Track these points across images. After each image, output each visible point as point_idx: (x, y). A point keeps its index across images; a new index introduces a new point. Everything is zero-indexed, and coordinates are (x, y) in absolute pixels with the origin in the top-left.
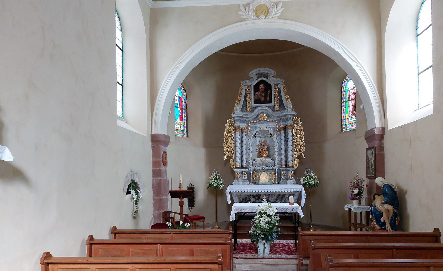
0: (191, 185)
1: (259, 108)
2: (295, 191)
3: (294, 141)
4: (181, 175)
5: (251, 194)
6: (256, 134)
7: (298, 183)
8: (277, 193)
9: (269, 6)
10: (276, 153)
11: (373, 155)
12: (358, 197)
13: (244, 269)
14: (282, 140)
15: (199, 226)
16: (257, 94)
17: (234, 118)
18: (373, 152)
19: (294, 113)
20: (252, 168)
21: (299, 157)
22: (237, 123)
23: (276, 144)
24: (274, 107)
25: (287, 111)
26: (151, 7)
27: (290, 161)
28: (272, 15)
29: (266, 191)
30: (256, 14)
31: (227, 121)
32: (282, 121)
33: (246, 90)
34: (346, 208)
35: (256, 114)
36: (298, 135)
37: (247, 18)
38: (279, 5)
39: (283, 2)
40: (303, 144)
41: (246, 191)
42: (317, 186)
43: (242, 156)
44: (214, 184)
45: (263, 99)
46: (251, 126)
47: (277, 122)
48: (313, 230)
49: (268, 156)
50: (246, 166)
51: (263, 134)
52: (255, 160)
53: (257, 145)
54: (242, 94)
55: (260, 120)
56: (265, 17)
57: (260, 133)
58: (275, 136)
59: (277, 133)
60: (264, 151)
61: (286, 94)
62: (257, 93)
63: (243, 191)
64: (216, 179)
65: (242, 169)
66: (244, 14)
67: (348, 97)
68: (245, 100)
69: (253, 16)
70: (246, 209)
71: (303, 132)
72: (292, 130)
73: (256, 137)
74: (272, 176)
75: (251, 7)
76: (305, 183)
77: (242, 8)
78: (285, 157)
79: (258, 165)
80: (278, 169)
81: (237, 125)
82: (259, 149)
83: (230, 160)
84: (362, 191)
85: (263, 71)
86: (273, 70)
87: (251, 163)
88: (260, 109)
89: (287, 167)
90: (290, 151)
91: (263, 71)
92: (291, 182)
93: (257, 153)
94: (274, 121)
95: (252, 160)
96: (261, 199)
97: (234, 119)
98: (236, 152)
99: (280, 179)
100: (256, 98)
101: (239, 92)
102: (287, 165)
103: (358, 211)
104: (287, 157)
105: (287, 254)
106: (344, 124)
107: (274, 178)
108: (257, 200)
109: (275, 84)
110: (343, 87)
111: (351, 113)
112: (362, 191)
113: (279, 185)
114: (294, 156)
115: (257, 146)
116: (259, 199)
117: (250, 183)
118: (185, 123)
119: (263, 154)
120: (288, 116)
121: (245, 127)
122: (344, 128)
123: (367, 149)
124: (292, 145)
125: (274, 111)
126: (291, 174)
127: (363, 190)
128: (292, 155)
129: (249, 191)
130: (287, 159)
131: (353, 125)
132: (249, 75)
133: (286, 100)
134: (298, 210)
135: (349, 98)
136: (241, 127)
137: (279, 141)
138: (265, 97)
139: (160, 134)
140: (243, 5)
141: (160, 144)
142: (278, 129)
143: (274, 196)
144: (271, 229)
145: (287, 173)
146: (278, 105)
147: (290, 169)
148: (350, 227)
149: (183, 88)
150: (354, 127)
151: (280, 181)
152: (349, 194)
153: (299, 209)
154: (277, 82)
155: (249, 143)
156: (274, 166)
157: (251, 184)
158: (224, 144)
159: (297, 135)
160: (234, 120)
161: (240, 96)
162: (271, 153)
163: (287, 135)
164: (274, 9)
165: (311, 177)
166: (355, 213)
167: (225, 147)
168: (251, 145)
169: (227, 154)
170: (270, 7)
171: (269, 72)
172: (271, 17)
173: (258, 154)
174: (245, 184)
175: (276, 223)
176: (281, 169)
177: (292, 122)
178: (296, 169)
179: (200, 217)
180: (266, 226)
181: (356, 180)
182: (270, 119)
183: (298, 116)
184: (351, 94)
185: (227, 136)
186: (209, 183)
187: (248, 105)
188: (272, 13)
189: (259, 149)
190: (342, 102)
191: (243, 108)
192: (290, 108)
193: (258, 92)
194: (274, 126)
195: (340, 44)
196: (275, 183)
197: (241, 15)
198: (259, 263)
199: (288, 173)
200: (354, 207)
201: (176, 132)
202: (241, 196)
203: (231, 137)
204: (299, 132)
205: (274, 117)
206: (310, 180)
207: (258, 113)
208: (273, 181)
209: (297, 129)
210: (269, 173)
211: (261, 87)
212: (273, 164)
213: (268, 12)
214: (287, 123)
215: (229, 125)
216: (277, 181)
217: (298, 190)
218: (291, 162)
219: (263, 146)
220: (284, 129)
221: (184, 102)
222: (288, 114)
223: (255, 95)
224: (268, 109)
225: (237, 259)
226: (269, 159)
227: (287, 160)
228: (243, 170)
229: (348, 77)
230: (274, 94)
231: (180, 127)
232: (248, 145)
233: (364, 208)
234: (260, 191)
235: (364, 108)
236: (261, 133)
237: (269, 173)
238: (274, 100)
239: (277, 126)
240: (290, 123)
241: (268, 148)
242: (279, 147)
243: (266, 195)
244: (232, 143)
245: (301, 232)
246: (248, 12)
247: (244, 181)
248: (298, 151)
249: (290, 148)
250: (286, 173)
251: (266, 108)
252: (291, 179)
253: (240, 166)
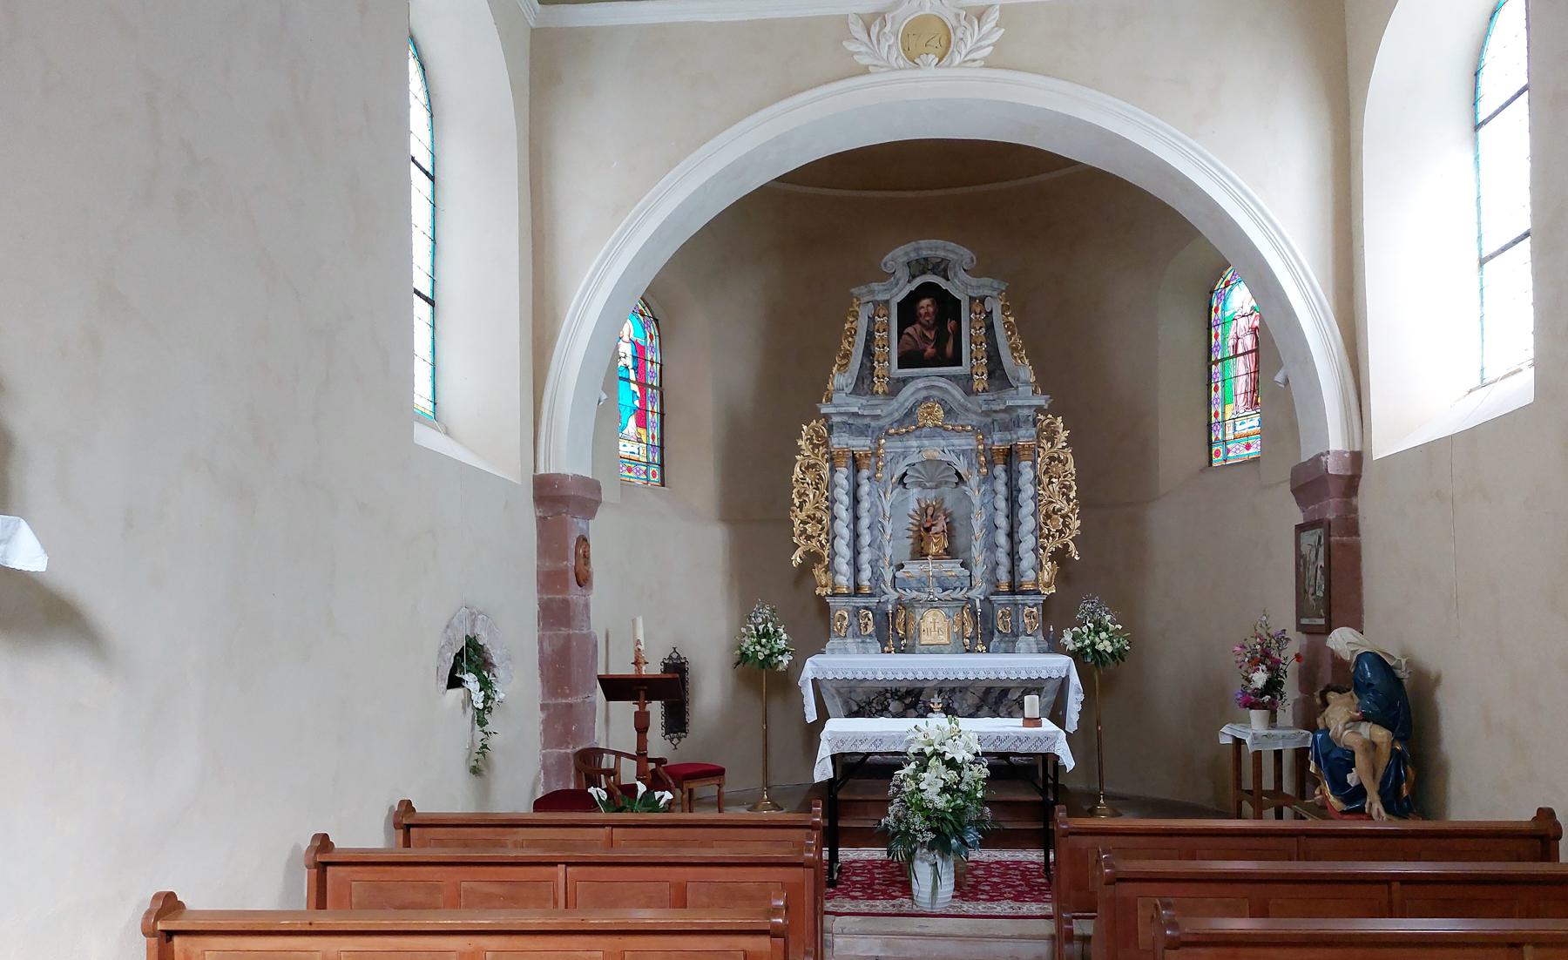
0: (675, 656)
1: (918, 381)
2: (1044, 675)
3: (1040, 501)
4: (640, 621)
5: (888, 685)
6: (905, 474)
7: (1055, 647)
8: (980, 684)
9: (951, 21)
10: (979, 542)
11: (1322, 550)
12: (1267, 698)
13: (863, 952)
14: (999, 496)
15: (705, 801)
16: (908, 334)
17: (827, 416)
18: (1320, 538)
19: (1041, 401)
20: (893, 595)
21: (1060, 556)
22: (837, 435)
23: (977, 510)
24: (970, 378)
25: (1017, 394)
26: (533, 25)
27: (1026, 571)
28: (963, 53)
29: (941, 677)
30: (906, 50)
31: (805, 427)
32: (997, 428)
33: (871, 319)
34: (1226, 736)
35: (907, 404)
36: (1055, 478)
37: (875, 63)
38: (988, 18)
39: (1003, 8)
40: (1072, 511)
41: (870, 676)
42: (1123, 660)
43: (856, 553)
44: (756, 652)
45: (930, 350)
46: (889, 446)
47: (980, 433)
48: (1109, 813)
49: (950, 553)
50: (870, 588)
52: (902, 566)
53: (911, 513)
54: (856, 332)
55: (920, 424)
56: (937, 59)
57: (920, 472)
58: (974, 480)
59: (979, 471)
60: (936, 533)
61: (1013, 334)
62: (909, 330)
63: (860, 676)
64: (766, 635)
65: (856, 599)
66: (863, 49)
67: (1231, 342)
68: (868, 353)
69: (895, 56)
70: (871, 740)
71: (1071, 467)
72: (1034, 462)
73: (907, 486)
74: (963, 624)
75: (889, 25)
76: (1081, 649)
77: (857, 29)
78: (1009, 554)
80: (982, 598)
81: (840, 441)
82: (916, 529)
83: (816, 565)
84: (1282, 677)
85: (929, 252)
86: (965, 250)
87: (888, 577)
88: (921, 385)
89: (1016, 590)
90: (1027, 534)
91: (929, 252)
92: (1029, 645)
93: (911, 541)
94: (970, 428)
95: (892, 568)
96: (925, 707)
97: (827, 421)
98: (834, 538)
99: (992, 634)
100: (908, 348)
101: (847, 326)
102: (1016, 584)
103: (1268, 749)
104: (1017, 557)
105: (1015, 899)
106: (1217, 439)
107: (969, 630)
108: (909, 708)
109: (972, 299)
110: (1213, 309)
111: (1241, 399)
112: (1282, 677)
113: (987, 654)
114: (1041, 551)
115: (910, 516)
116: (917, 703)
117: (886, 649)
118: (653, 437)
119: (930, 544)
120: (1019, 411)
121: (868, 449)
122: (1217, 454)
123: (1300, 529)
124: (1034, 515)
125: (969, 392)
126: (1030, 615)
127: (1285, 672)
128: (1035, 550)
129: (880, 676)
130: (1016, 563)
131: (1250, 442)
132: (882, 265)
133: (1012, 354)
134: (1054, 745)
135: (1235, 347)
136: (854, 449)
137: (986, 501)
138: (940, 343)
139: (566, 476)
140: (861, 16)
141: (568, 511)
142: (983, 459)
143: (970, 694)
144: (958, 812)
145: (1017, 613)
146: (985, 371)
147: (1025, 597)
148: (1240, 803)
149: (647, 313)
150: (1252, 451)
151: (991, 641)
152: (1236, 686)
153: (1058, 741)
155: (880, 507)
156: (971, 589)
157: (890, 652)
158: (793, 512)
159: (1051, 477)
160: (829, 425)
161: (850, 339)
162: (960, 541)
163: (1017, 480)
164: (968, 34)
165: (1099, 627)
166: (1258, 755)
167: (797, 522)
168: (888, 515)
169: (803, 545)
170: (955, 23)
171: (951, 256)
172: (958, 60)
173: (912, 544)
174: (866, 652)
175: (975, 789)
176: (993, 598)
177: (1033, 431)
178: (1048, 597)
179: (707, 768)
180: (941, 802)
181: (1260, 636)
182: (956, 421)
183: (1054, 410)
184: (1242, 334)
185: (803, 483)
186: (740, 650)
187: (878, 371)
188: (963, 46)
189: (916, 529)
190: (1209, 363)
191: (860, 383)
192: (1027, 383)
193: (915, 326)
194: (970, 445)
195: (1204, 157)
196: (972, 648)
197: (852, 54)
198: (918, 930)
199: (1020, 612)
200: (1254, 734)
201: (624, 469)
202: (853, 695)
203: (817, 484)
204: (1057, 467)
205: (970, 415)
206: (1097, 639)
207: (912, 401)
208: (968, 640)
209: (1052, 459)
210: (951, 614)
211: (923, 307)
212: (966, 582)
213: (949, 42)
214: (1015, 436)
215: (811, 443)
216: (980, 641)
217: (1055, 675)
218: (1031, 575)
219: (932, 516)
220: (1007, 456)
221: (652, 362)
222: (1019, 403)
223: (903, 336)
224: (949, 388)
225: (838, 918)
226: (953, 565)
227: (1016, 568)
228: (860, 602)
229: (1233, 274)
230: (971, 335)
231: (637, 452)
232: (877, 514)
233: (1289, 738)
234: (920, 676)
235: (1287, 382)
236: (923, 472)
237: (951, 614)
238: (971, 353)
239: (980, 447)
240: (1028, 437)
241: (947, 523)
242: (986, 522)
243: (940, 692)
244: (820, 507)
245: (1066, 823)
246: (878, 41)
247: (863, 642)
248: (1053, 536)
249: (1028, 524)
250: (1013, 614)
251: (943, 383)
252: (1030, 635)
253: (848, 588)
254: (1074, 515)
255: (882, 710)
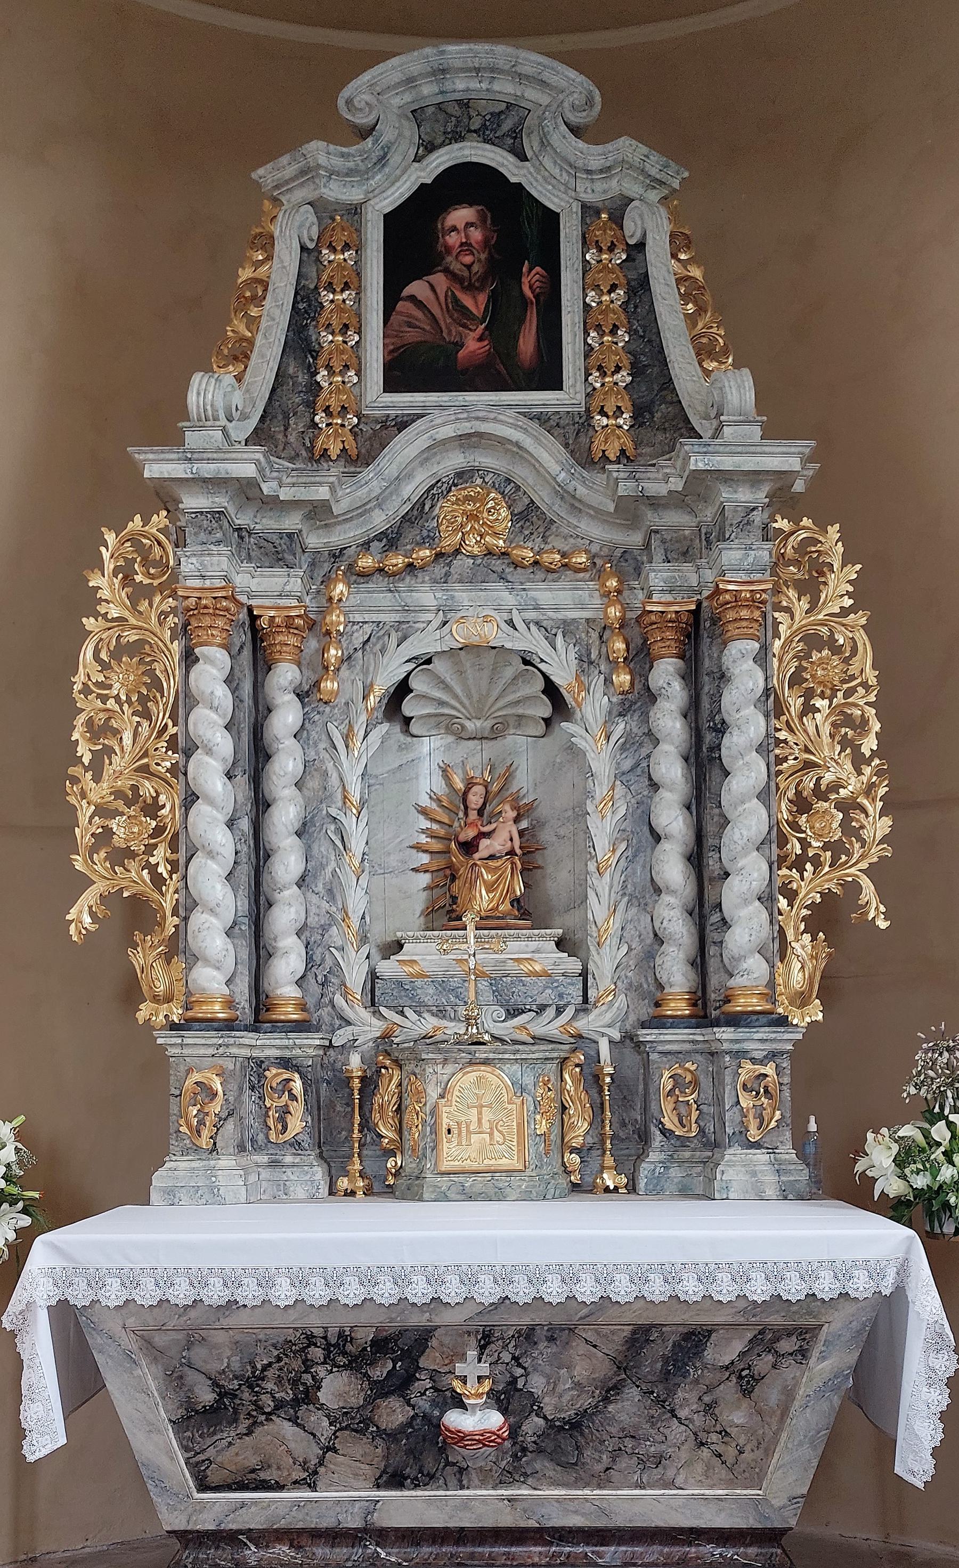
2: (826, 1287)
3: (780, 760)
5: (315, 1323)
6: (403, 689)
8: (611, 1314)
10: (607, 877)
14: (664, 747)
16: (412, 298)
23: (601, 790)
24: (584, 423)
29: (487, 1292)
31: (110, 537)
32: (658, 556)
40: (869, 790)
41: (249, 1293)
50: (303, 1007)
51: (476, 697)
52: (398, 946)
53: (425, 801)
54: (266, 290)
57: (447, 687)
59: (608, 681)
61: (701, 310)
62: (417, 288)
63: (215, 1294)
65: (249, 1038)
72: (765, 649)
73: (414, 728)
74: (564, 1108)
79: (428, 1000)
80: (617, 1036)
82: (437, 846)
85: (474, 84)
86: (572, 74)
87: (356, 977)
88: (448, 431)
89: (714, 1014)
90: (745, 852)
91: (474, 84)
92: (754, 1174)
95: (365, 950)
99: (644, 1138)
100: (412, 336)
104: (715, 918)
108: (386, 1395)
109: (589, 211)
114: (783, 903)
115: (424, 812)
116: (409, 1379)
117: (343, 1183)
119: (472, 885)
124: (764, 796)
126: (756, 1086)
128: (767, 899)
129: (284, 1294)
130: (712, 936)
132: (341, 102)
136: (253, 602)
142: (620, 645)
143: (583, 1348)
145: (717, 1080)
146: (626, 404)
147: (741, 1033)
154: (614, 183)
155: (334, 780)
156: (586, 1011)
157: (353, 1193)
158: (75, 780)
159: (809, 695)
161: (254, 312)
163: (716, 698)
167: (85, 812)
168: (355, 796)
171: (532, 94)
173: (428, 888)
174: (281, 1194)
176: (647, 1035)
177: (763, 554)
182: (545, 539)
185: (104, 698)
189: (437, 846)
191: (277, 428)
193: (431, 278)
199: (728, 1079)
202: (198, 1355)
203: (143, 700)
208: (575, 1158)
209: (812, 641)
210: (528, 1080)
211: (454, 229)
215: (128, 580)
216: (609, 1161)
217: (861, 1286)
219: (481, 812)
222: (727, 463)
223: (400, 306)
224: (528, 443)
226: (533, 945)
227: (712, 950)
232: (325, 796)
234: (419, 1291)
236: (458, 690)
237: (528, 1080)
238: (587, 356)
240: (749, 572)
241: (521, 833)
242: (627, 825)
243: (486, 1340)
244: (153, 767)
247: (274, 1164)
248: (817, 862)
250: (705, 1082)
252: (757, 1145)
253: (229, 1003)
254: (874, 800)
255: (296, 1403)
